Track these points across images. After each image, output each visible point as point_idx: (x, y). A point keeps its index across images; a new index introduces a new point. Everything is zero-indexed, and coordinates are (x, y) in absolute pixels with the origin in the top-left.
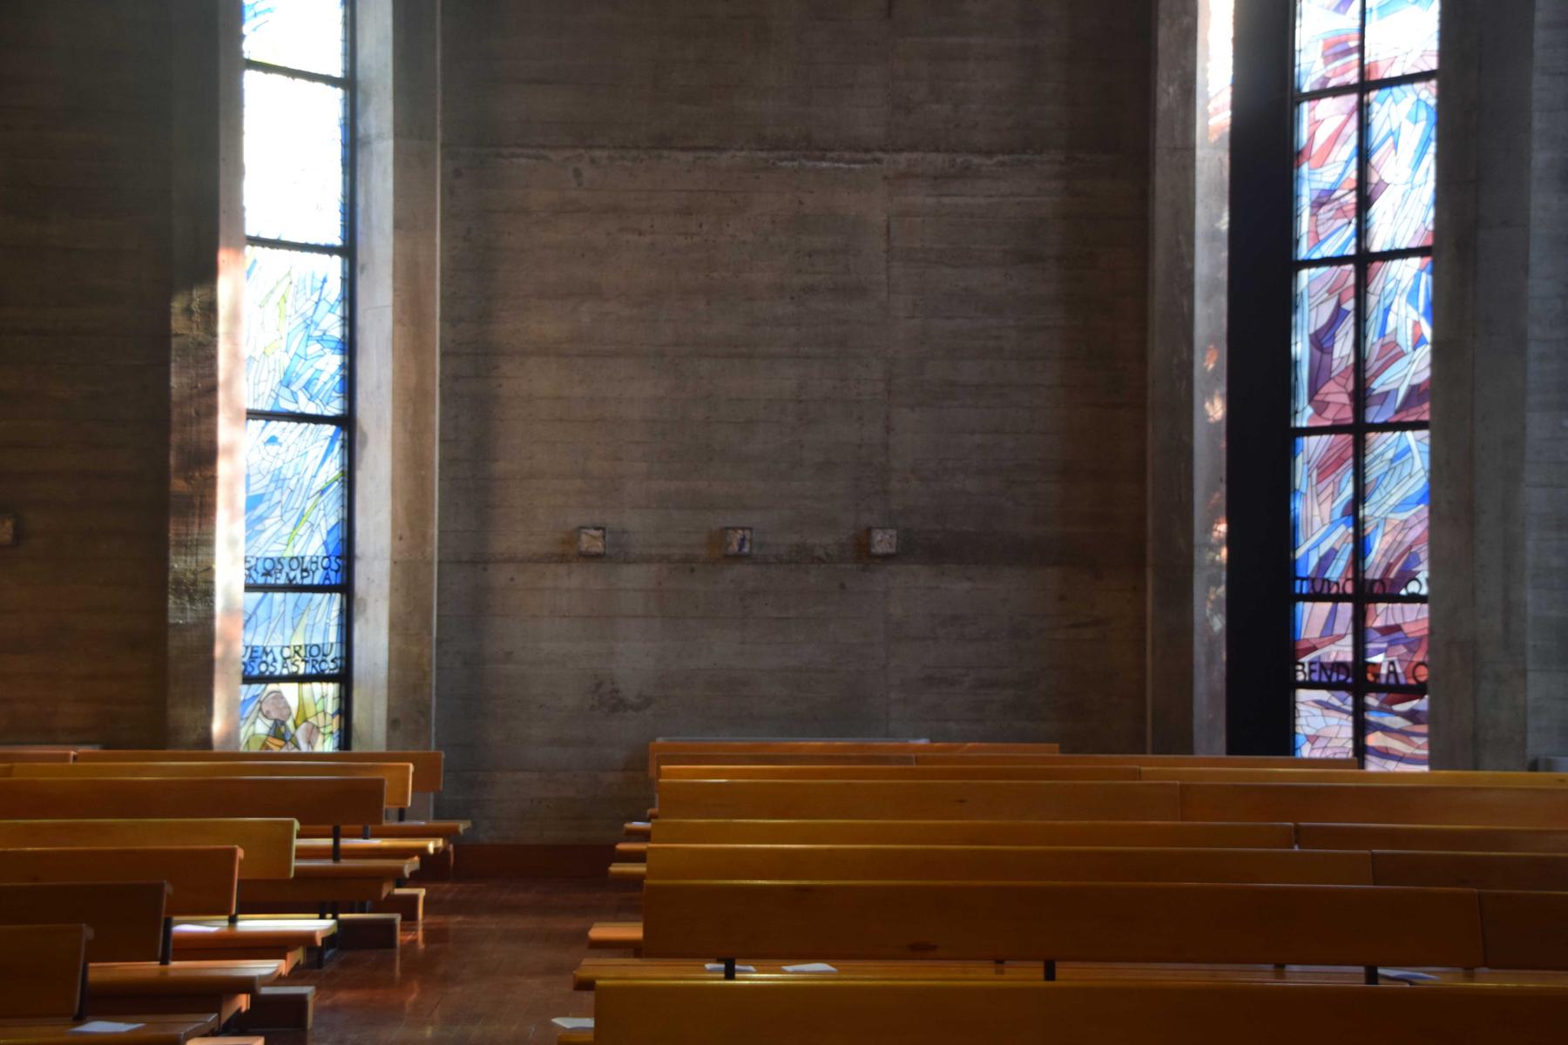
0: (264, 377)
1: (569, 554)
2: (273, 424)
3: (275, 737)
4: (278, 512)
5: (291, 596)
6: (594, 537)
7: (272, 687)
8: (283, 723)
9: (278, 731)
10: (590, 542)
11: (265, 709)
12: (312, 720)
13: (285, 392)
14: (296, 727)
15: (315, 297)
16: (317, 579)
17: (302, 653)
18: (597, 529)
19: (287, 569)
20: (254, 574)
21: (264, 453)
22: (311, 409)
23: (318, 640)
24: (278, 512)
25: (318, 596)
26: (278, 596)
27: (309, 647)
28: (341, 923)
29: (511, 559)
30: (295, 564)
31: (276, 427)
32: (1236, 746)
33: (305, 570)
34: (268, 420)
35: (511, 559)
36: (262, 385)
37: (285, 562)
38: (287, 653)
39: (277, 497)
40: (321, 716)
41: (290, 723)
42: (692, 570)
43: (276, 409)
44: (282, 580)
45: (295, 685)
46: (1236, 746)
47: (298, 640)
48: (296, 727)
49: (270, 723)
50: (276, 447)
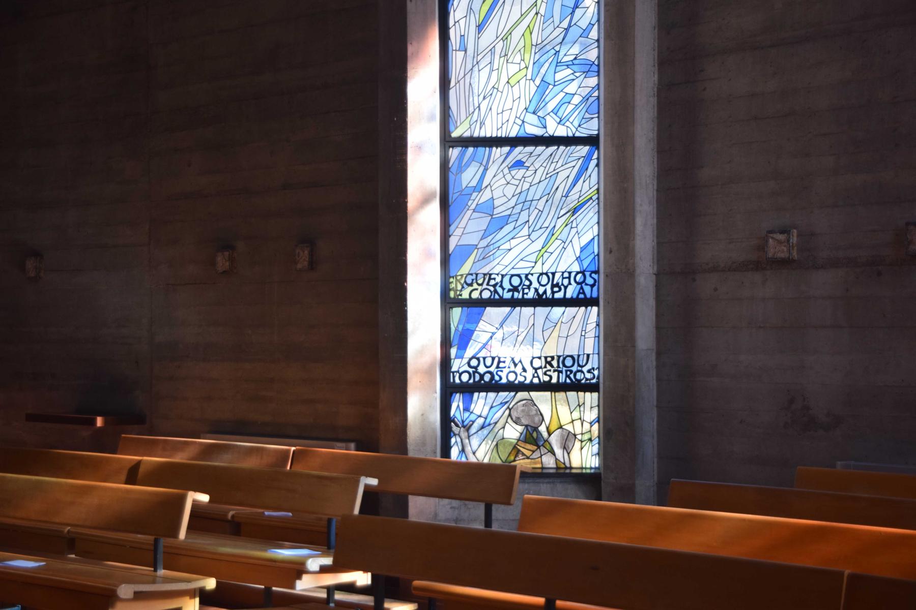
0: (508, 105)
1: (761, 264)
2: (519, 149)
3: (526, 441)
4: (525, 231)
5: (542, 311)
6: (780, 242)
7: (521, 395)
8: (536, 429)
9: (533, 438)
10: (776, 249)
11: (514, 415)
12: (569, 428)
13: (530, 118)
14: (550, 434)
15: (565, 24)
16: (572, 292)
17: (555, 363)
18: (782, 232)
19: (535, 284)
20: (499, 290)
21: (508, 177)
22: (561, 132)
23: (572, 350)
24: (525, 231)
25: (571, 311)
26: (527, 311)
27: (562, 359)
28: (293, 587)
29: (715, 269)
30: (544, 280)
31: (520, 152)
32: (442, 457)
33: (557, 285)
34: (491, 147)
35: (715, 269)
36: (506, 114)
37: (534, 279)
38: (537, 363)
39: (524, 217)
40: (578, 424)
41: (542, 429)
42: (879, 274)
43: (522, 134)
44: (531, 295)
45: (548, 394)
46: (442, 457)
47: (551, 350)
48: (550, 434)
49: (520, 428)
50: (522, 171)
